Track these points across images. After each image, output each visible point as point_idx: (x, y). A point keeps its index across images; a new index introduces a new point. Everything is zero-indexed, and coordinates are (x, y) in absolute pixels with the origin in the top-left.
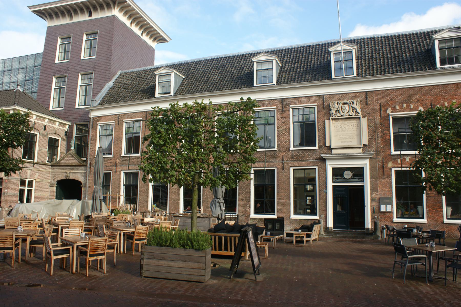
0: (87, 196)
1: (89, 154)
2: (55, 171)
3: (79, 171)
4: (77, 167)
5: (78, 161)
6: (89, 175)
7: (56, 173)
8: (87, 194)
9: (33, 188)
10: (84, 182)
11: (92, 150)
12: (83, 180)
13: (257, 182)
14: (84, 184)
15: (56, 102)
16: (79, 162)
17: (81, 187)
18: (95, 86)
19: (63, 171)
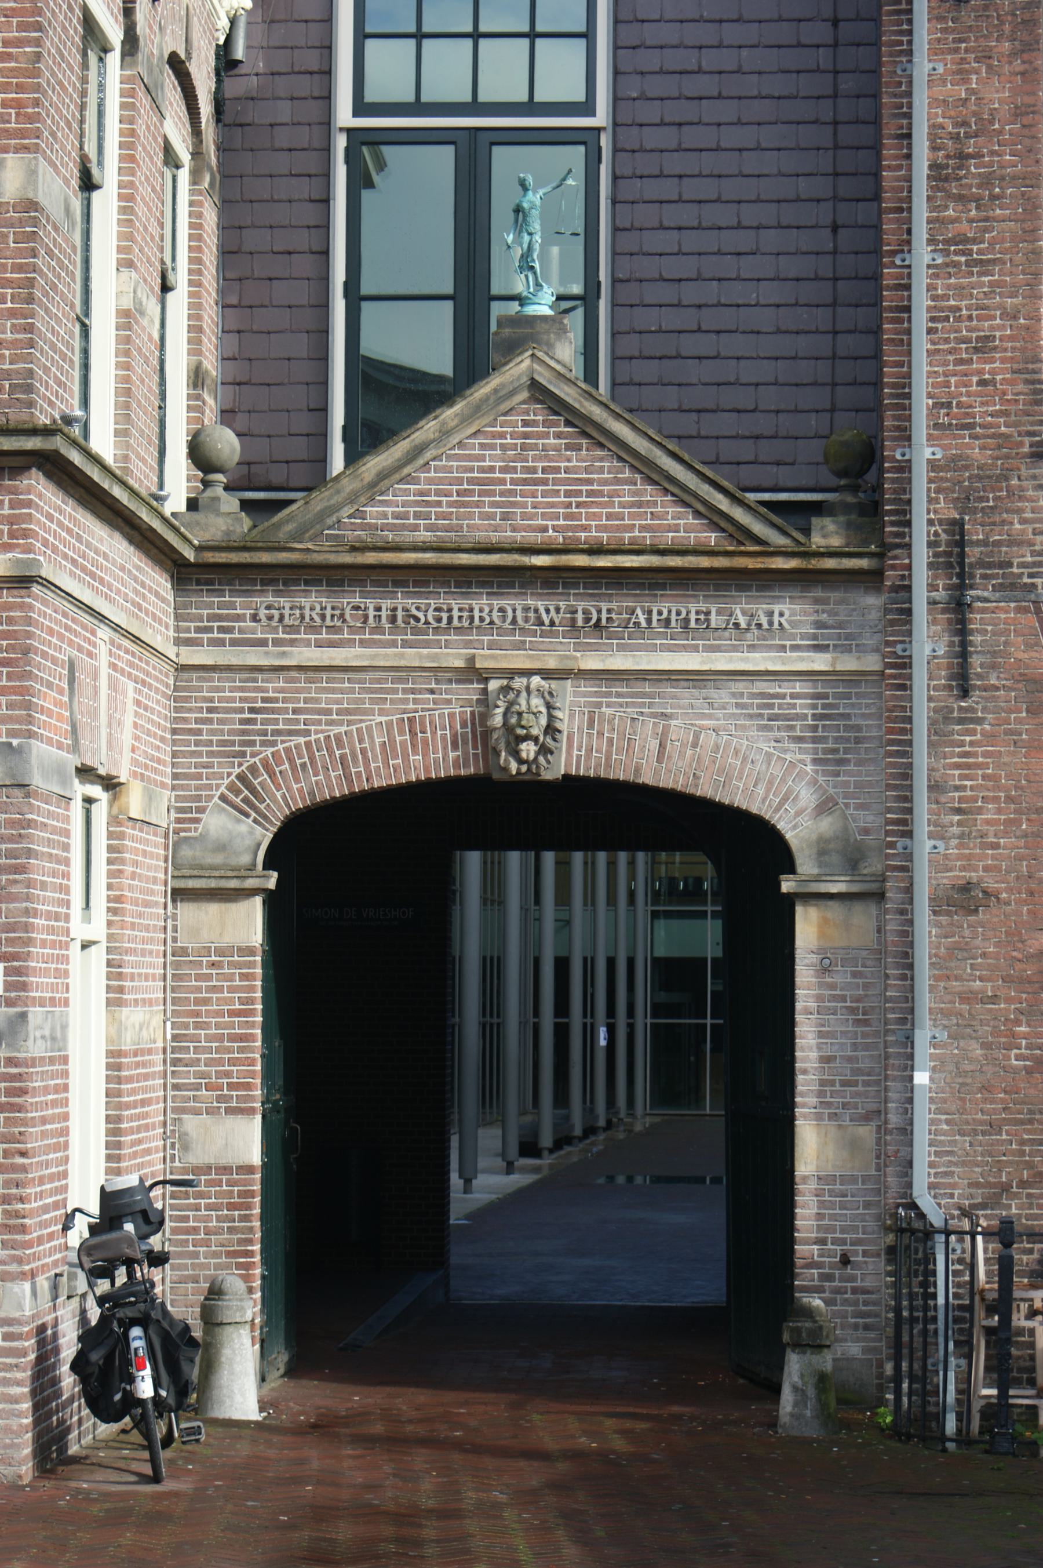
0: (923, 1037)
1: (921, 404)
2: (253, 657)
3: (722, 662)
4: (665, 606)
5: (684, 497)
6: (941, 719)
7: (273, 686)
8: (925, 1001)
9: (926, 682)
10: (826, 825)
11: (984, 346)
12: (807, 797)
13: (820, 867)
14: (822, 849)
15: (91, 533)
16: (714, 518)
17: (790, 901)
18: (303, 422)
19: (412, 657)
